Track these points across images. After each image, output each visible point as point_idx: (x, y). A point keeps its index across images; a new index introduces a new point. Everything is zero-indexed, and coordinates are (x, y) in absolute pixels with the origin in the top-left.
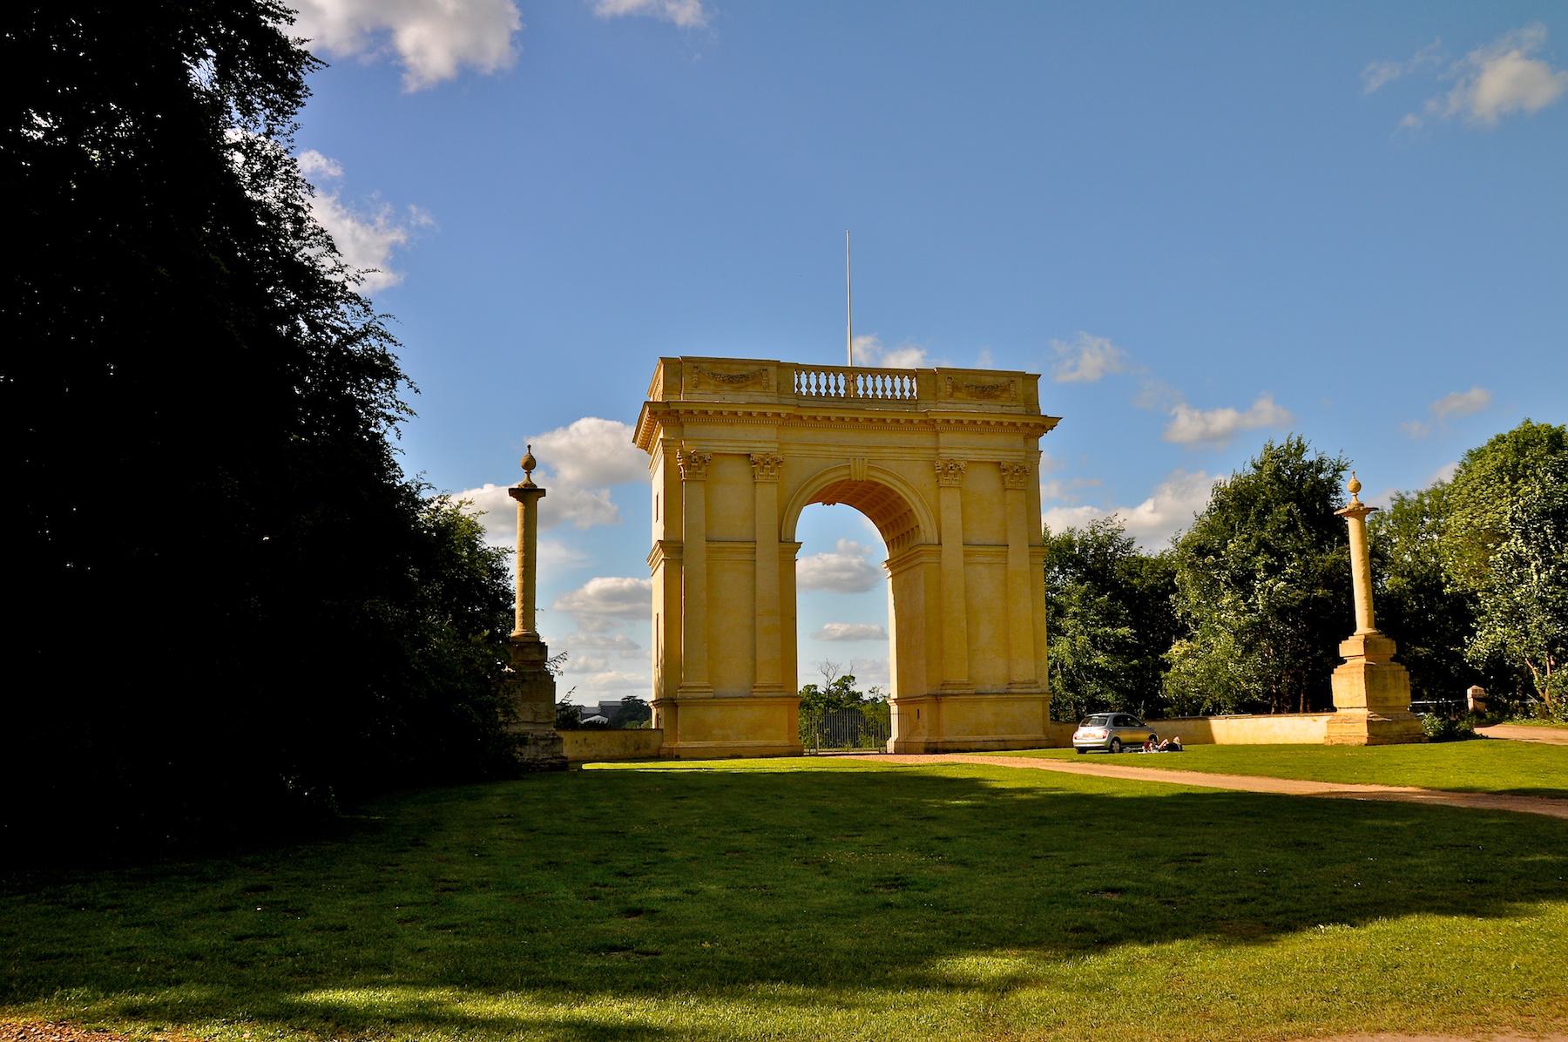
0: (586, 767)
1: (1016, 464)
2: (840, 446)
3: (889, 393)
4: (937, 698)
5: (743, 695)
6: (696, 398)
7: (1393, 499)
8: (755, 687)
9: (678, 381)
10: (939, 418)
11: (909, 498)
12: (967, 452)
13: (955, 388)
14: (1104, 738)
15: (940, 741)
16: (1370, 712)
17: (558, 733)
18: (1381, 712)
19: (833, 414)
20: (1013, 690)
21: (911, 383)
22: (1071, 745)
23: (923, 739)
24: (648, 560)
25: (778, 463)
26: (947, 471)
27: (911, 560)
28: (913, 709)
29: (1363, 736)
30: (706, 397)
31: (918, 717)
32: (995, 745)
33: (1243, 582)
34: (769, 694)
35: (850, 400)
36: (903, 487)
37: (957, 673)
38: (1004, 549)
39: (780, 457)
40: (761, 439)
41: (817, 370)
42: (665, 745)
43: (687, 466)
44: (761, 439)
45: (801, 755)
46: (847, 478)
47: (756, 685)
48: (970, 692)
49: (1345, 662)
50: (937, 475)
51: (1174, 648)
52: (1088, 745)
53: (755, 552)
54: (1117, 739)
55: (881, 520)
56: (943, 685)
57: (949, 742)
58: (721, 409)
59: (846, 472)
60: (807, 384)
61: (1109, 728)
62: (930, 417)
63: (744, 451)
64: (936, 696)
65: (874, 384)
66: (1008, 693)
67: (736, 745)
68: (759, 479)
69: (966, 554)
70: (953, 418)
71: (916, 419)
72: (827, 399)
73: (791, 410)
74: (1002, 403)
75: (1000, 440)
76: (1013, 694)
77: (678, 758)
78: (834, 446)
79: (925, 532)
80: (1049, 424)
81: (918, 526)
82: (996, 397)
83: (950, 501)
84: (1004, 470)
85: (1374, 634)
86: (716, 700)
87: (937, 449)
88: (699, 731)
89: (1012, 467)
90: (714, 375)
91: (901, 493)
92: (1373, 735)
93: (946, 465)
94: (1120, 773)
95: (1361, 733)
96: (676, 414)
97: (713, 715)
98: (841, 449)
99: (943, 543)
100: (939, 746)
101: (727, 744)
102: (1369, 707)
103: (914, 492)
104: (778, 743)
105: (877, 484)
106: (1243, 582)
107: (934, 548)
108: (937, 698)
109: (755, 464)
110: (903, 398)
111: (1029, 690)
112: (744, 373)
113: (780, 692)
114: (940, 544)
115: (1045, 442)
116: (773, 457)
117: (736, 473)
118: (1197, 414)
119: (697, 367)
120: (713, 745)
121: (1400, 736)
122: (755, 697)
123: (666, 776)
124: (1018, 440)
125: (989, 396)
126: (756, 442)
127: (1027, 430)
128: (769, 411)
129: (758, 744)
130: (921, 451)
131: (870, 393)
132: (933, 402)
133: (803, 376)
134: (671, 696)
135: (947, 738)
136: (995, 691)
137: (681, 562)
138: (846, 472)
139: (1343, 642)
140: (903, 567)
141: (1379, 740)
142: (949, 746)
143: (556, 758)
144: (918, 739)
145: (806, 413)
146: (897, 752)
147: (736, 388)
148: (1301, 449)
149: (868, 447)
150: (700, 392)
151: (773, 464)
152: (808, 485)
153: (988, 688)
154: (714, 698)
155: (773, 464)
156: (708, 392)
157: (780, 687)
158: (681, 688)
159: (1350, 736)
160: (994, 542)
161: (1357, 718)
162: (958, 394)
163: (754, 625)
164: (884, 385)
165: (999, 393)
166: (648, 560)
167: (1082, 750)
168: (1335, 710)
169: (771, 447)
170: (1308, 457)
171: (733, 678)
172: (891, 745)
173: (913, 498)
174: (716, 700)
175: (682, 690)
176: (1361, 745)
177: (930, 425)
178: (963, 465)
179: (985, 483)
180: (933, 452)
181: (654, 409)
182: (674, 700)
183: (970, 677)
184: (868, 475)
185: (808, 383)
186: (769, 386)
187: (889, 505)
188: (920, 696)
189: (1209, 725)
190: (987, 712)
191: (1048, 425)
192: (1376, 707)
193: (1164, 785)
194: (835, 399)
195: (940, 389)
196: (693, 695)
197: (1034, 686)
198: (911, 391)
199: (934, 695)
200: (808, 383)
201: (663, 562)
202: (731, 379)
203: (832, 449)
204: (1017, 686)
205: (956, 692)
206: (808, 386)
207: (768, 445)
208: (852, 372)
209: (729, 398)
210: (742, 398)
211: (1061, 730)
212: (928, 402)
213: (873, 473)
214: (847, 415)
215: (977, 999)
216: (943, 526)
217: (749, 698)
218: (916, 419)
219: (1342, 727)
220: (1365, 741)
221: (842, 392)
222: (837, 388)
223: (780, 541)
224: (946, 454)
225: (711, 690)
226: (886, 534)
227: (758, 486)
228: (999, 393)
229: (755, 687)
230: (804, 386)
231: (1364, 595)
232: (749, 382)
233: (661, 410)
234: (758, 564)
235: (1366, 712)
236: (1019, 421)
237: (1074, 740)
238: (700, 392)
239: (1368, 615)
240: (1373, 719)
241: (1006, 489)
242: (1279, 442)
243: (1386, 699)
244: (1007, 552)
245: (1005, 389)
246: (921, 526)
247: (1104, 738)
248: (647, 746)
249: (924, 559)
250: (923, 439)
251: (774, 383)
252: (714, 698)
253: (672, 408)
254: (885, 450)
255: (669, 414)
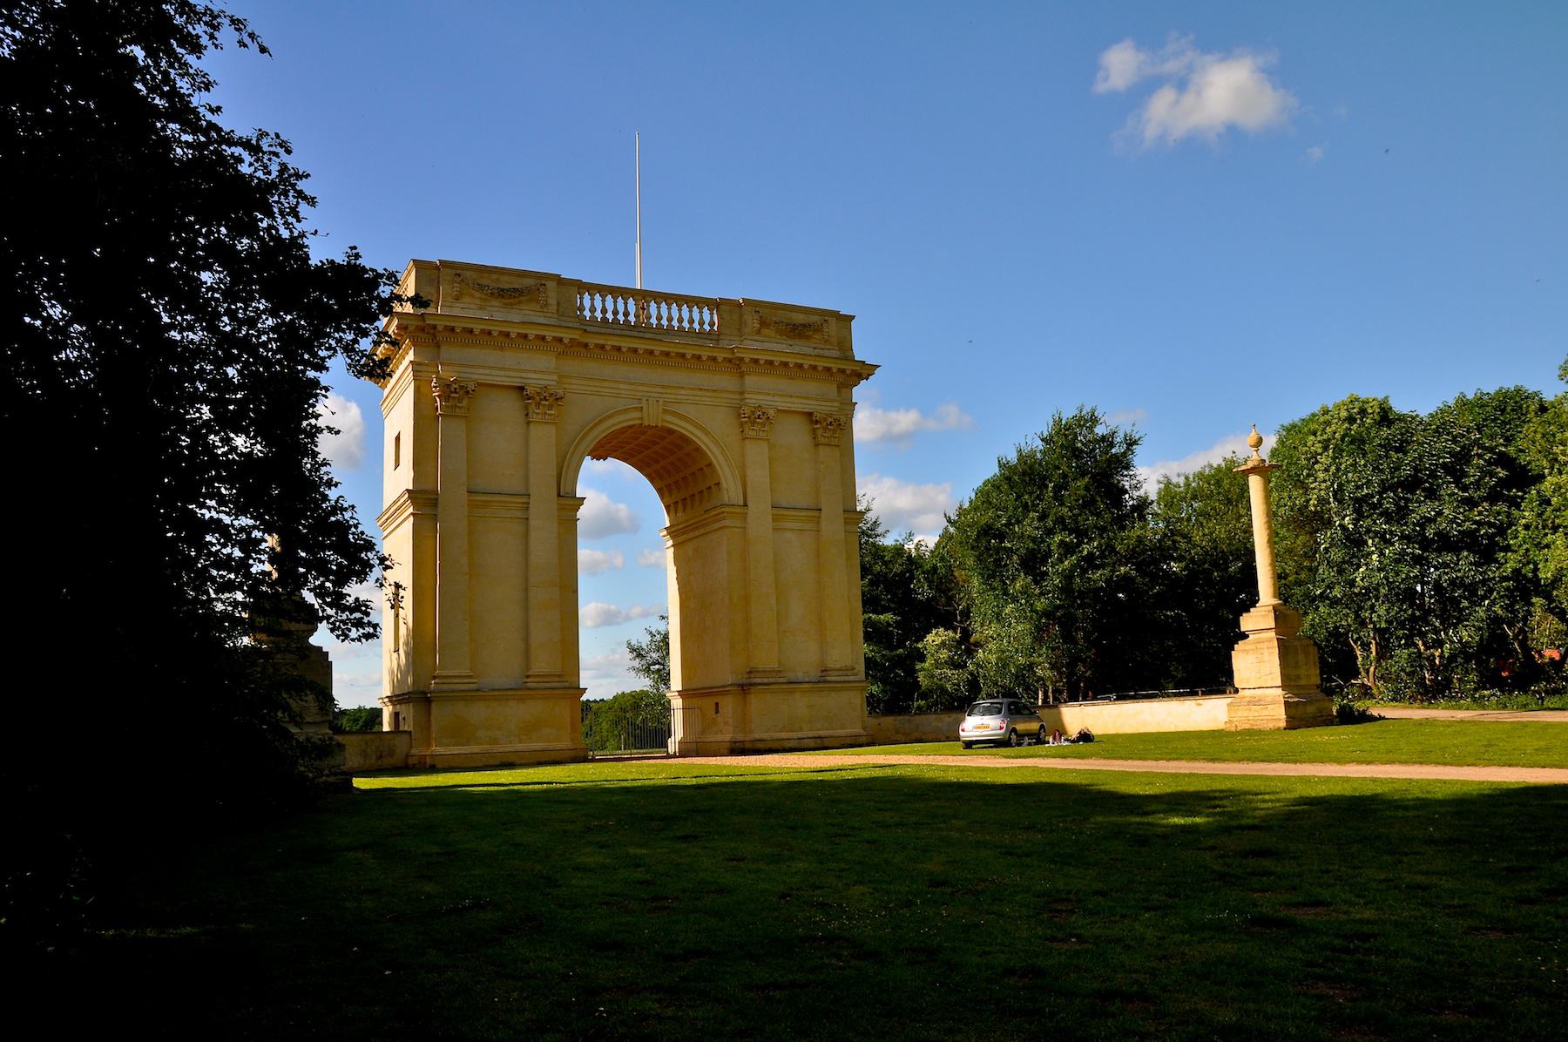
0: (360, 783)
1: (830, 415)
2: (631, 384)
3: (686, 325)
4: (744, 688)
5: (513, 686)
6: (456, 312)
7: (1160, 482)
8: (528, 677)
9: (433, 291)
10: (747, 356)
11: (709, 448)
12: (776, 398)
13: (764, 323)
14: (1001, 728)
15: (748, 739)
16: (1284, 692)
17: (336, 737)
18: (1295, 692)
19: (625, 344)
20: (828, 679)
21: (712, 314)
22: (958, 739)
23: (728, 737)
24: (379, 519)
25: (557, 399)
26: (753, 420)
27: (718, 520)
28: (709, 703)
29: (1280, 720)
30: (468, 310)
31: (717, 712)
32: (811, 743)
33: (1033, 563)
34: (547, 685)
35: (641, 329)
36: (704, 437)
37: (765, 658)
38: (816, 513)
39: (561, 392)
40: (537, 369)
41: (604, 290)
42: (414, 751)
43: (445, 396)
44: (537, 369)
45: (585, 760)
46: (638, 422)
47: (530, 673)
48: (782, 680)
49: (1247, 636)
50: (742, 424)
51: (930, 638)
52: (974, 739)
53: (527, 509)
54: (1014, 730)
55: (661, 479)
56: (751, 672)
57: (760, 740)
58: (490, 328)
59: (638, 415)
60: (591, 306)
61: (1005, 716)
62: (737, 355)
63: (517, 382)
64: (742, 686)
65: (670, 313)
66: (823, 680)
67: (507, 750)
68: (533, 417)
69: (775, 518)
70: (762, 357)
71: (720, 356)
72: (615, 326)
73: (576, 335)
74: (815, 346)
75: (811, 387)
76: (829, 682)
77: (433, 769)
78: (625, 383)
79: (727, 490)
80: (864, 371)
81: (718, 484)
82: (808, 338)
83: (757, 454)
84: (817, 422)
85: (1280, 605)
86: (477, 694)
87: (742, 393)
88: (459, 733)
89: (825, 420)
90: (481, 287)
91: (700, 444)
92: (1290, 717)
93: (753, 413)
94: (1090, 764)
95: (1278, 715)
96: (432, 331)
97: (477, 712)
98: (632, 387)
99: (749, 503)
100: (748, 745)
101: (497, 748)
102: (1283, 687)
103: (717, 443)
104: (560, 745)
105: (671, 432)
106: (1033, 563)
107: (738, 510)
108: (744, 688)
109: (529, 399)
110: (701, 333)
111: (846, 678)
112: (517, 286)
113: (559, 682)
114: (745, 505)
115: (860, 392)
116: (552, 392)
117: (505, 409)
118: (880, 412)
119: (459, 275)
120: (478, 751)
121: (1315, 718)
122: (530, 689)
123: (515, 799)
124: (831, 390)
125: (801, 336)
126: (531, 371)
127: (841, 378)
128: (549, 334)
129: (534, 748)
130: (724, 395)
131: (664, 322)
132: (736, 338)
133: (587, 297)
134: (421, 689)
135: (757, 736)
136: (807, 680)
137: (435, 518)
138: (638, 415)
139: (1244, 615)
140: (692, 535)
141: (1297, 723)
142: (760, 745)
143: (335, 774)
144: (720, 738)
145: (593, 341)
146: (683, 754)
147: (506, 304)
148: (1094, 420)
149: (663, 387)
150: (461, 305)
151: (551, 400)
152: (592, 428)
153: (800, 676)
154: (478, 690)
155: (551, 400)
156: (472, 306)
157: (559, 676)
158: (434, 678)
159: (1262, 720)
160: (805, 506)
161: (1269, 699)
162: (765, 331)
163: (526, 599)
164: (680, 315)
165: (810, 333)
166: (379, 519)
167: (969, 745)
168: (1236, 691)
169: (550, 380)
170: (1100, 430)
171: (501, 666)
172: (673, 745)
173: (715, 449)
174: (477, 694)
175: (437, 681)
176: (1279, 729)
177: (736, 365)
178: (771, 413)
179: (794, 435)
180: (737, 396)
181: (405, 322)
182: (426, 694)
183: (779, 662)
184: (663, 420)
185: (592, 305)
186: (546, 305)
187: (688, 454)
188: (723, 686)
189: (1059, 714)
190: (801, 704)
191: (865, 373)
192: (1289, 685)
193: (1464, 783)
194: (624, 327)
195: (745, 323)
196: (452, 687)
197: (850, 673)
198: (712, 324)
199: (740, 685)
200: (592, 305)
201: (411, 518)
202: (502, 293)
203: (622, 386)
204: (834, 673)
205: (766, 681)
206: (593, 310)
207: (546, 377)
208: (644, 296)
209: (498, 316)
210: (515, 316)
211: (879, 724)
212: (732, 338)
213: (668, 418)
214: (641, 346)
215: (413, 741)
216: (749, 484)
217: (522, 690)
218: (720, 356)
219: (1250, 710)
220: (1283, 724)
221: (632, 318)
222: (626, 314)
223: (559, 495)
224: (753, 400)
225: (475, 681)
226: (667, 494)
227: (531, 425)
228: (810, 333)
229: (528, 677)
230: (587, 309)
231: (1270, 561)
232: (524, 298)
233: (413, 324)
234: (533, 523)
235: (1280, 691)
236: (835, 366)
237: (961, 733)
238: (461, 305)
239: (1274, 584)
240: (1289, 700)
241: (817, 445)
242: (1068, 414)
243: (1298, 677)
244: (819, 517)
245: (818, 329)
246: (724, 485)
247: (1001, 728)
248: (391, 754)
249: (727, 522)
250: (726, 381)
251: (553, 302)
252: (478, 690)
253: (427, 322)
254: (683, 392)
255: (423, 330)
